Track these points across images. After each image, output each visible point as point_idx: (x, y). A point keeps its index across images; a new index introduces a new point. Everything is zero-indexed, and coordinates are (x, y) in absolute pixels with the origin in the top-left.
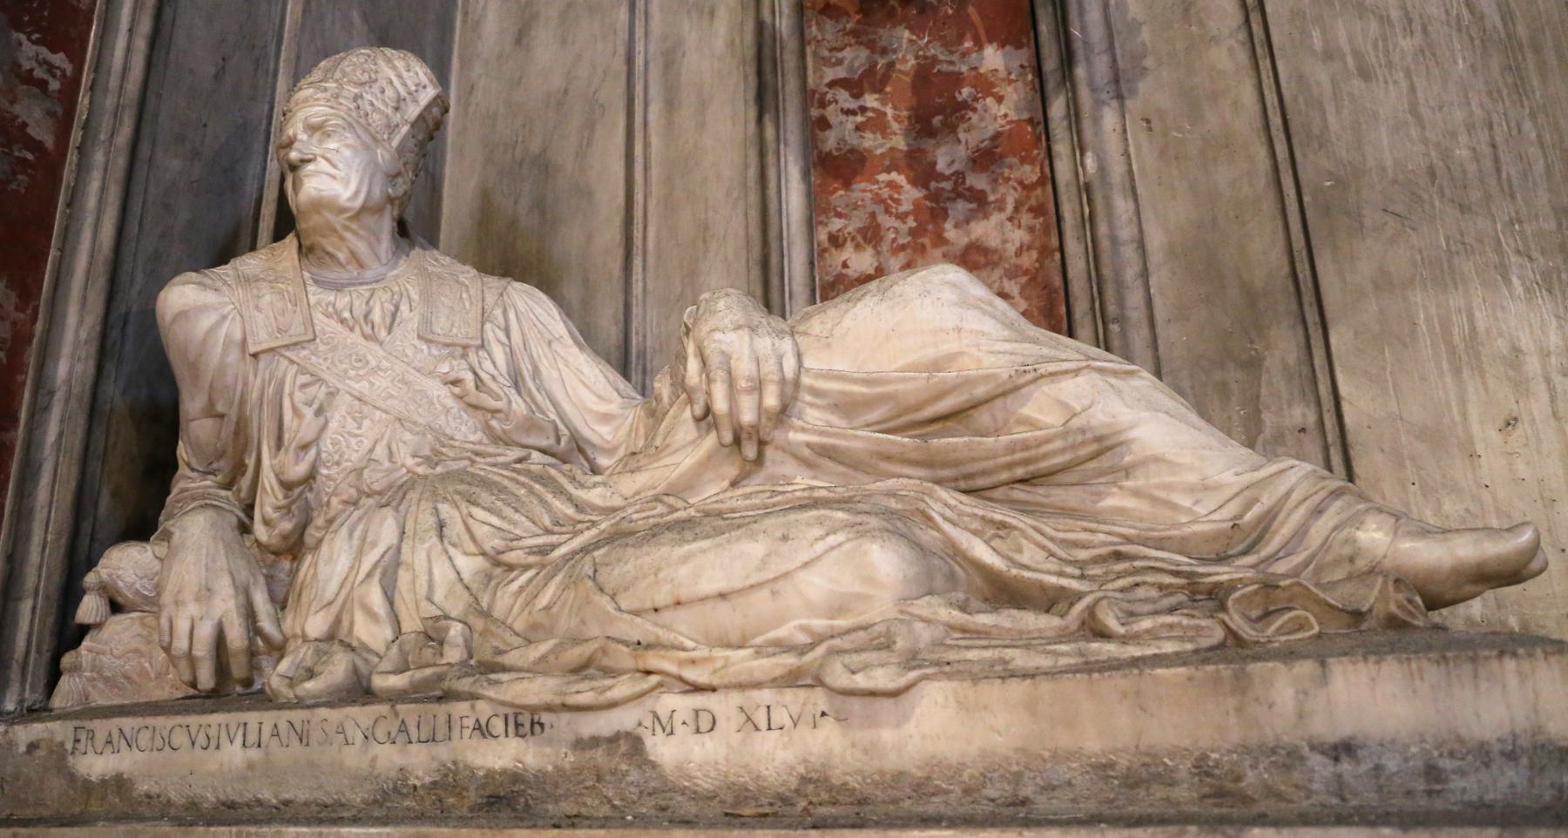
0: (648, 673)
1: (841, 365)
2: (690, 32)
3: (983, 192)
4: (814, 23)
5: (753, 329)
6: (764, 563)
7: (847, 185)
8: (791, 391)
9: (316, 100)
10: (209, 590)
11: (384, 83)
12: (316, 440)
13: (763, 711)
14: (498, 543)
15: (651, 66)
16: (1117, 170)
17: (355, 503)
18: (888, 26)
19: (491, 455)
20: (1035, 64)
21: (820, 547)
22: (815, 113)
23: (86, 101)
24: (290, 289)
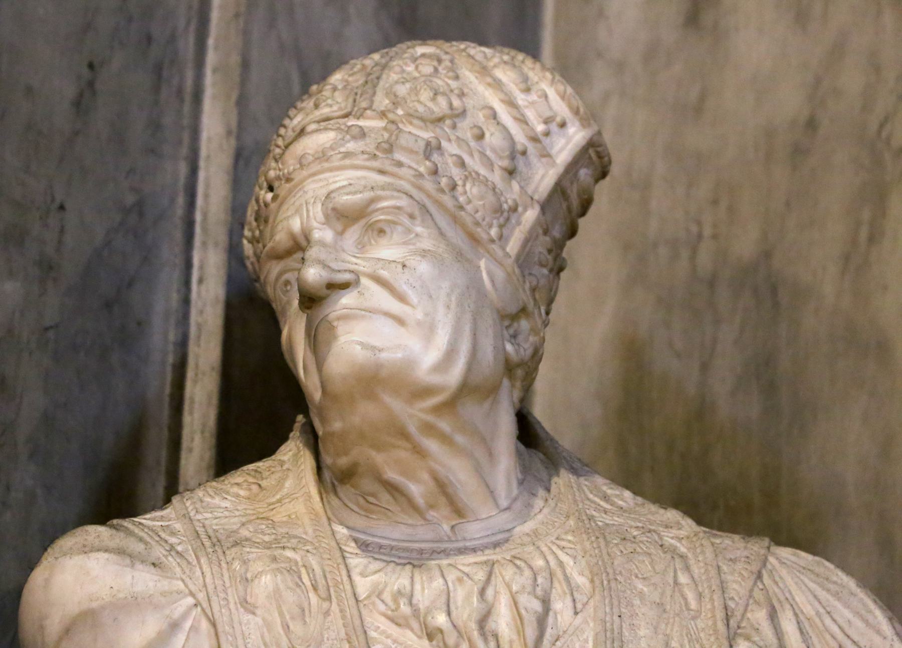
9: (347, 155)
11: (480, 117)
24: (314, 562)
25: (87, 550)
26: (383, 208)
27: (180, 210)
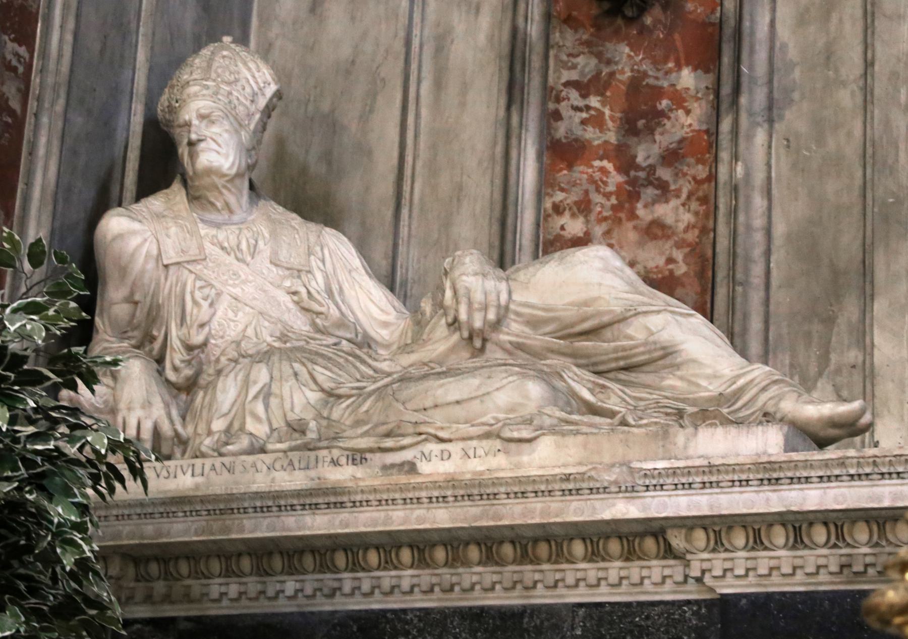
0: (420, 434)
1: (533, 300)
2: (459, 22)
3: (667, 182)
4: (558, 30)
5: (484, 275)
6: (479, 387)
7: (570, 167)
8: (504, 312)
9: (204, 95)
10: (149, 402)
12: (209, 322)
13: (472, 450)
14: (333, 385)
15: (425, 47)
16: (759, 177)
17: (236, 361)
18: (614, 41)
19: (320, 340)
20: (716, 87)
21: (505, 381)
22: (551, 106)
23: (38, 80)
24: (187, 224)
25: (120, 215)
27: (129, 89)
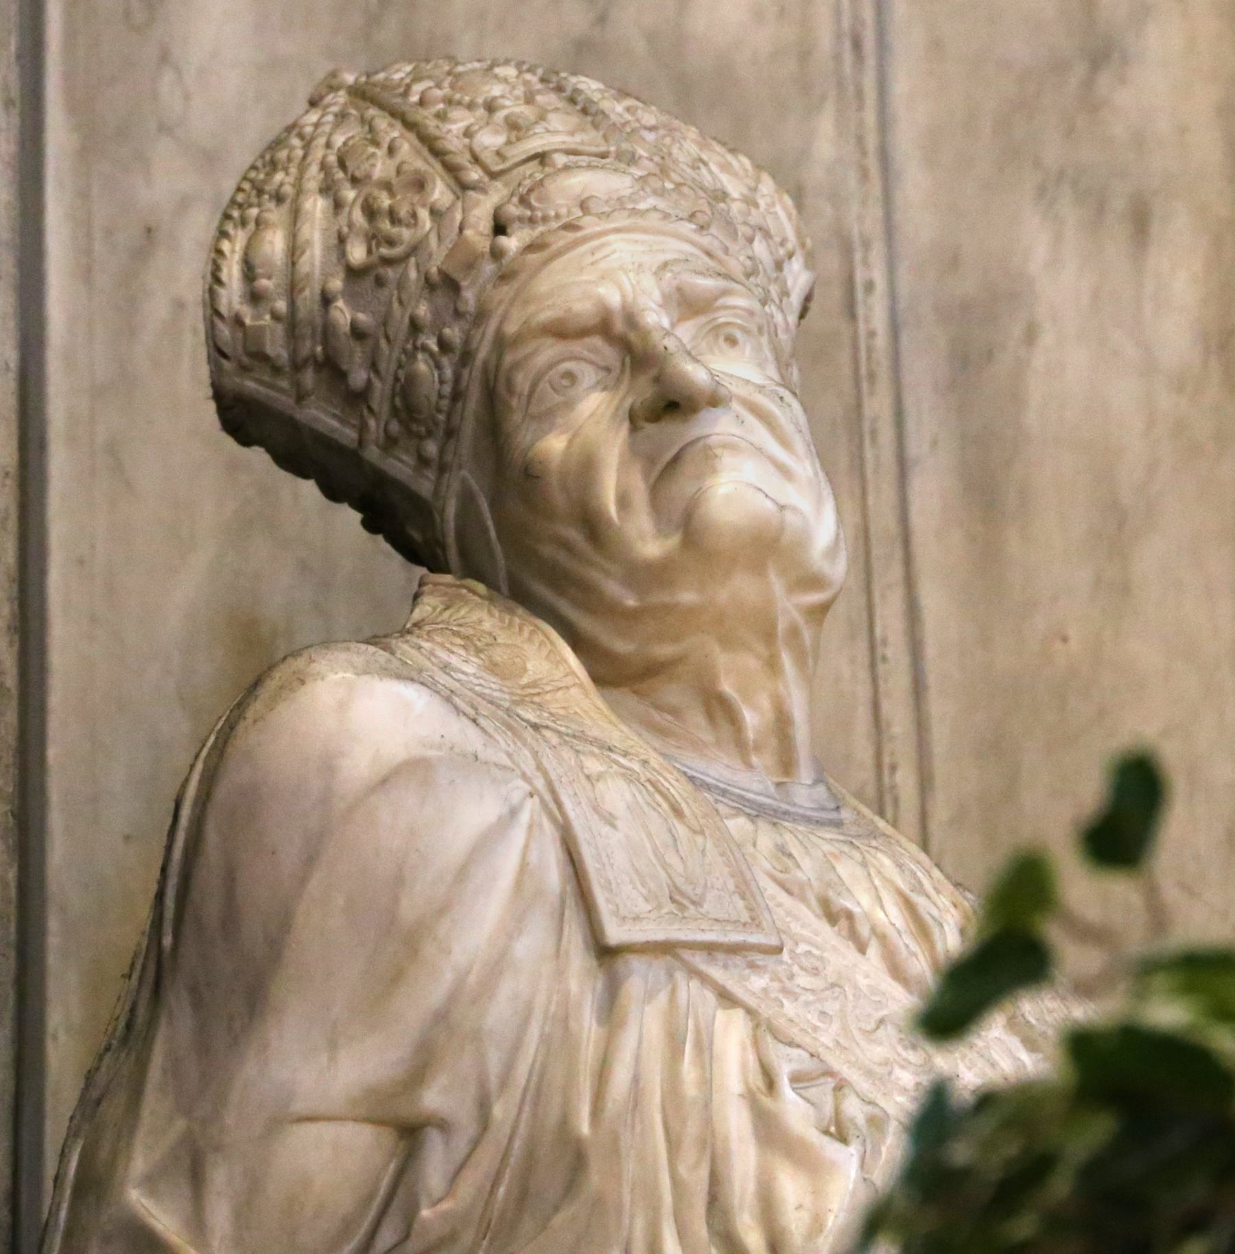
26: (734, 307)
